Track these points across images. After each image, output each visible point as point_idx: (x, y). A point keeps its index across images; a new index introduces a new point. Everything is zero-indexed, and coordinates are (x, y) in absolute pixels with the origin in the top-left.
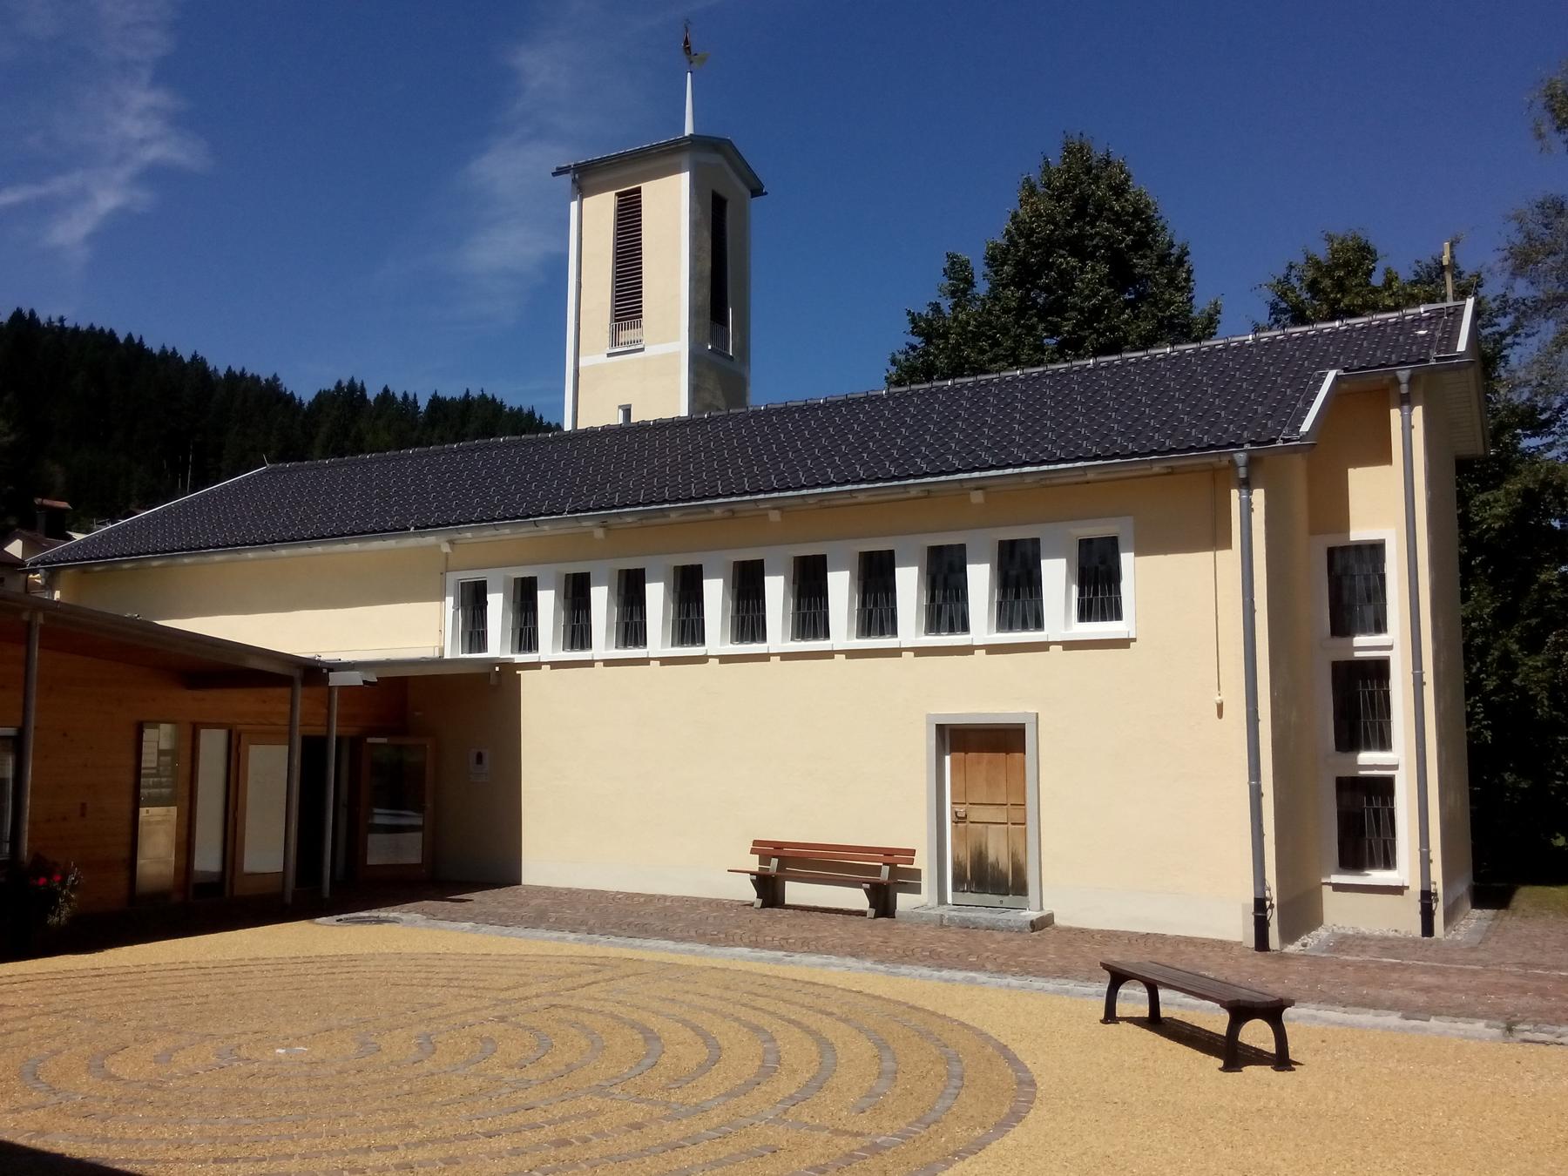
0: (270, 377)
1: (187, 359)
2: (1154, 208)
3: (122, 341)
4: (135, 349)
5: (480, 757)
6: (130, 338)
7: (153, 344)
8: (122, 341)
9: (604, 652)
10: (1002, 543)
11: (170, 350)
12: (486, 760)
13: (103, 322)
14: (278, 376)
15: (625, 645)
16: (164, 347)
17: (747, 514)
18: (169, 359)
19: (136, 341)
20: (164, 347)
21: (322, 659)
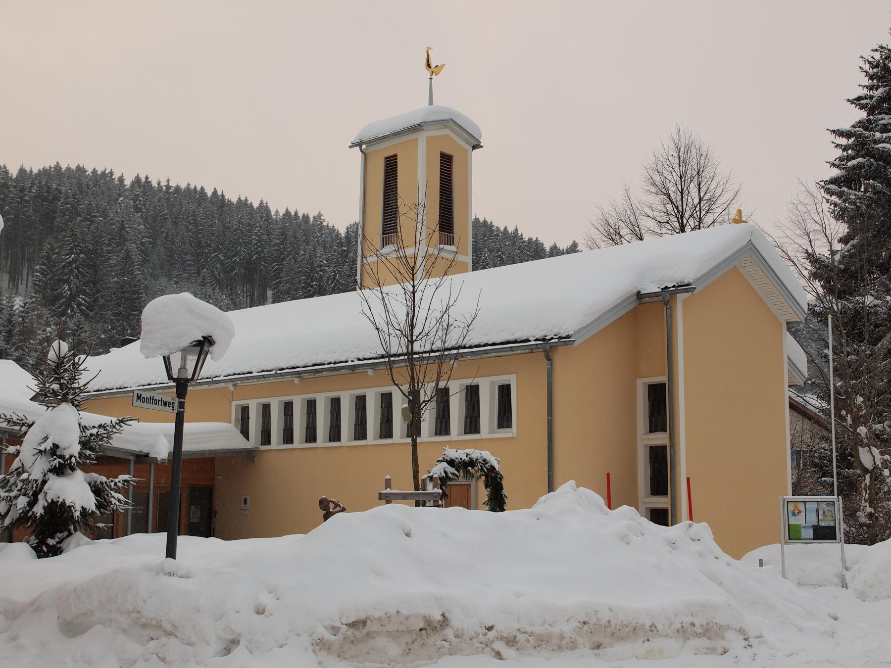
0: (316, 214)
1: (256, 205)
2: (150, 620)
3: (209, 195)
4: (219, 201)
5: (245, 500)
6: (215, 192)
7: (232, 196)
8: (209, 195)
9: (792, 497)
10: (650, 386)
11: (243, 198)
12: (248, 502)
13: (196, 183)
14: (148, 176)
15: (667, 494)
16: (287, 210)
17: (402, 262)
18: (243, 204)
19: (143, 180)
20: (287, 210)
21: (422, 423)
